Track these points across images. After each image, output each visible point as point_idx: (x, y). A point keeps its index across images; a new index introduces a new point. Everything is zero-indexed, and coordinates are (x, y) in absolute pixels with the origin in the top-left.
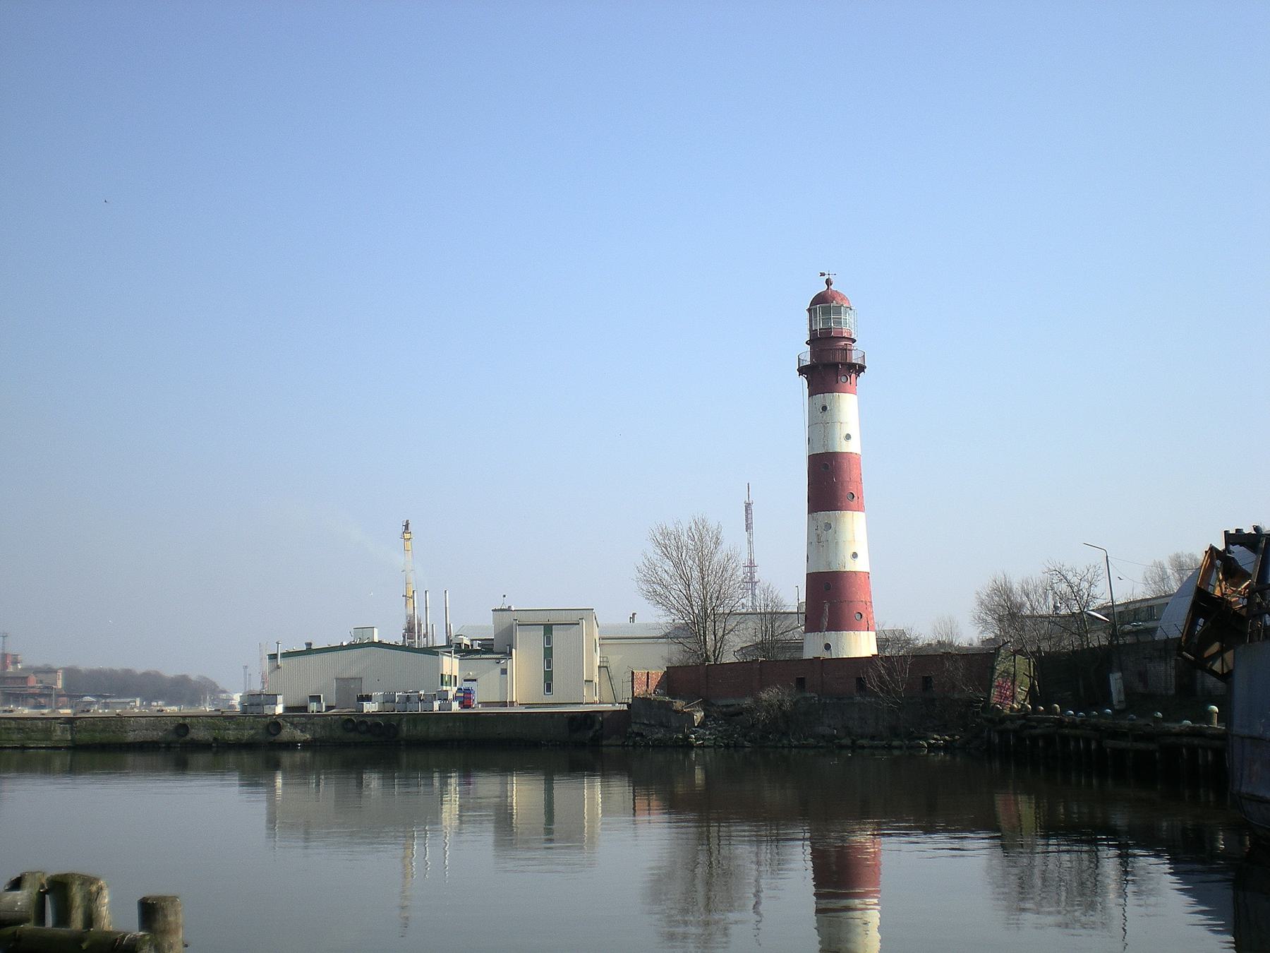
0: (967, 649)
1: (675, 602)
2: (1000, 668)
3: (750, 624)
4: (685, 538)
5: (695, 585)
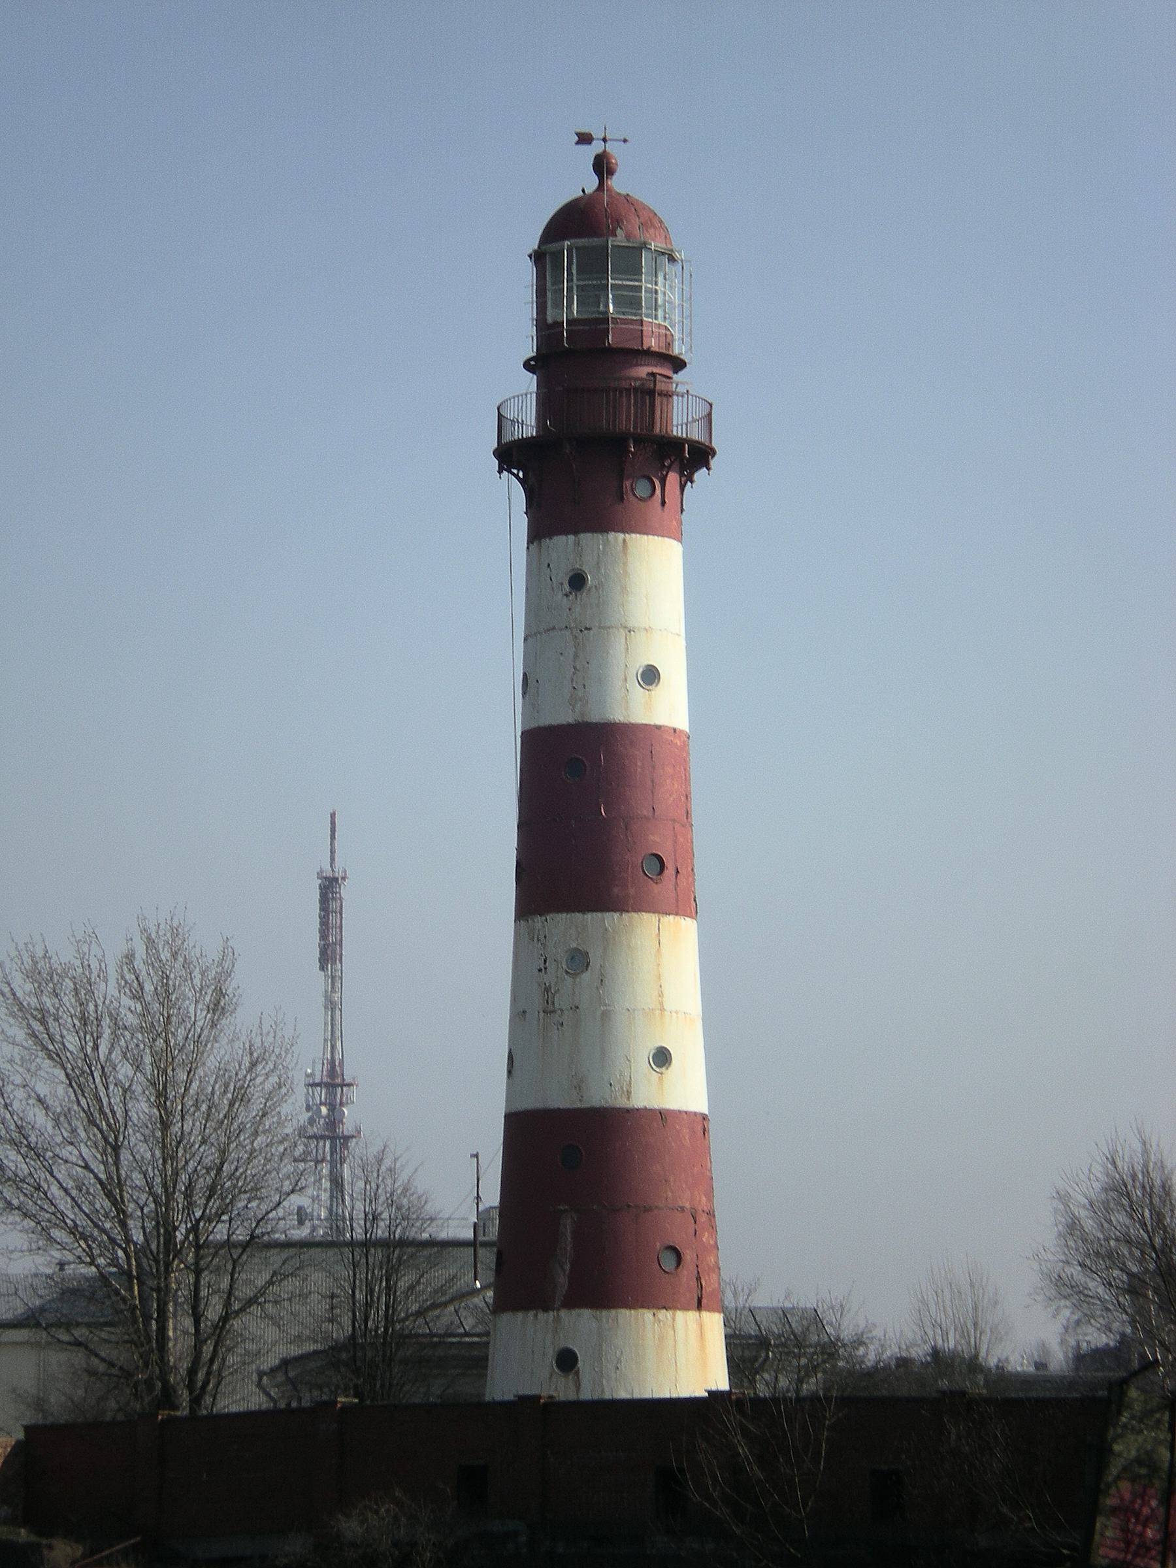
0: (1024, 1381)
1: (65, 1204)
2: (1126, 1448)
3: (318, 1281)
4: (109, 989)
5: (139, 1148)
